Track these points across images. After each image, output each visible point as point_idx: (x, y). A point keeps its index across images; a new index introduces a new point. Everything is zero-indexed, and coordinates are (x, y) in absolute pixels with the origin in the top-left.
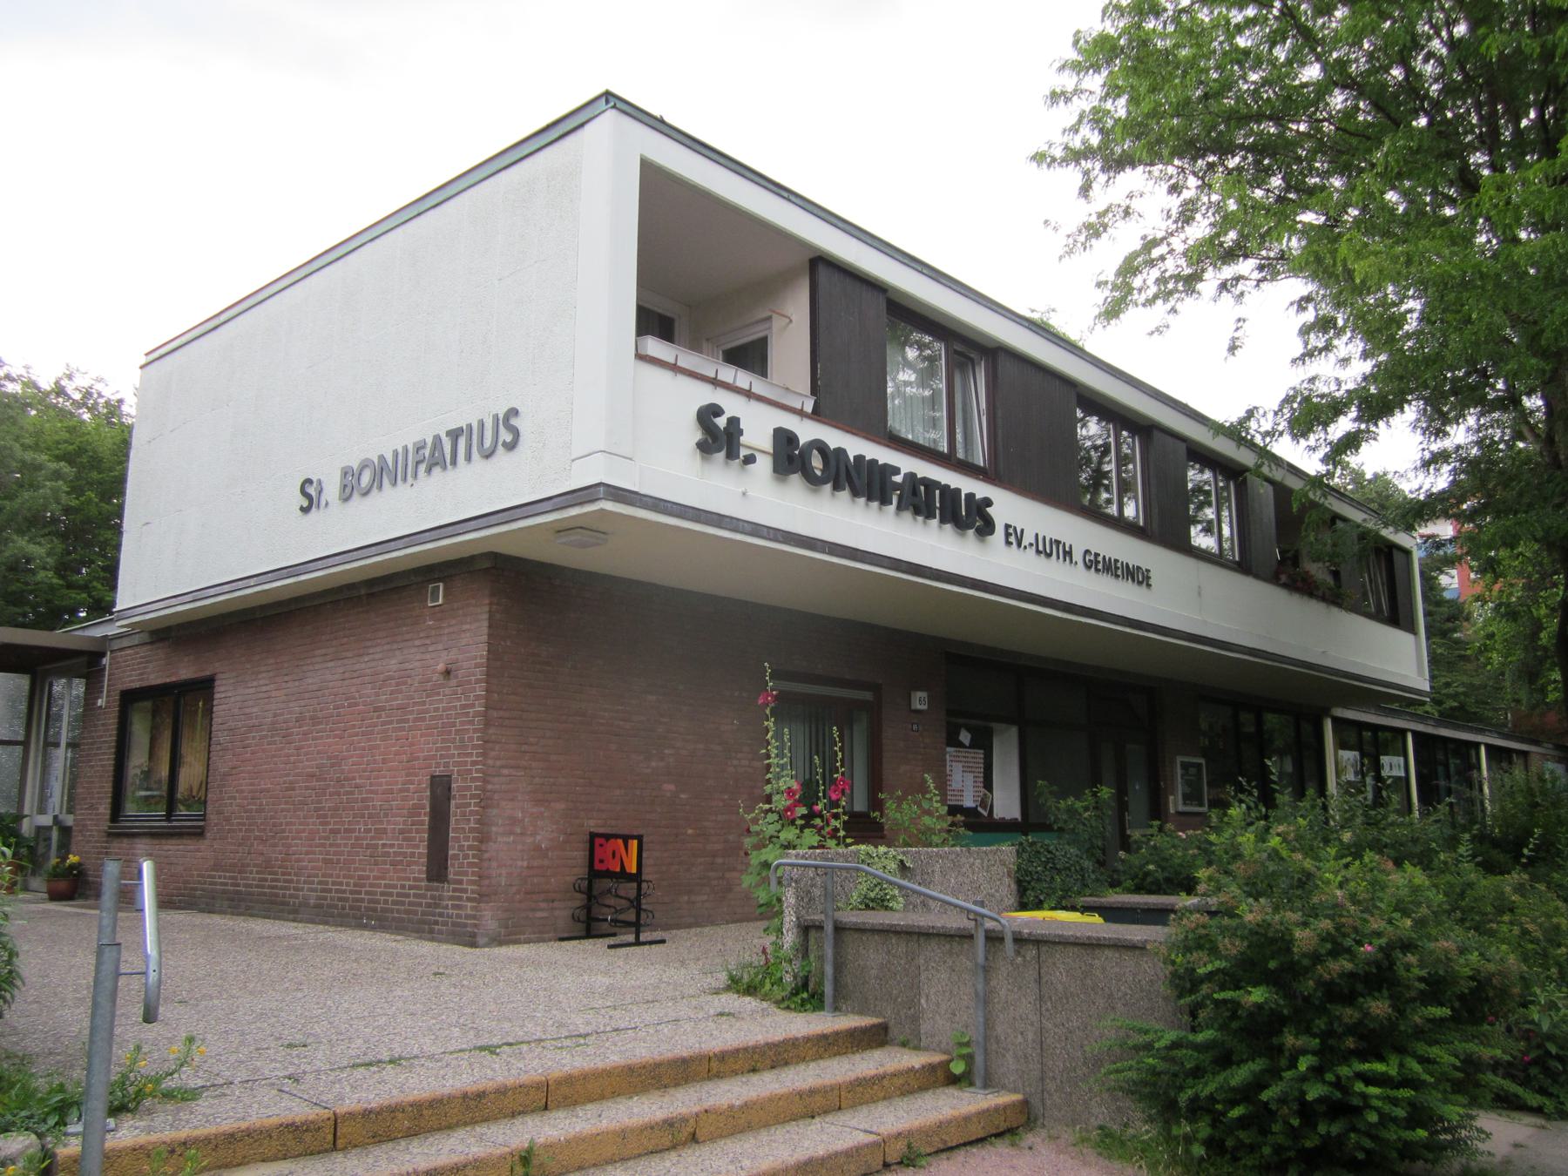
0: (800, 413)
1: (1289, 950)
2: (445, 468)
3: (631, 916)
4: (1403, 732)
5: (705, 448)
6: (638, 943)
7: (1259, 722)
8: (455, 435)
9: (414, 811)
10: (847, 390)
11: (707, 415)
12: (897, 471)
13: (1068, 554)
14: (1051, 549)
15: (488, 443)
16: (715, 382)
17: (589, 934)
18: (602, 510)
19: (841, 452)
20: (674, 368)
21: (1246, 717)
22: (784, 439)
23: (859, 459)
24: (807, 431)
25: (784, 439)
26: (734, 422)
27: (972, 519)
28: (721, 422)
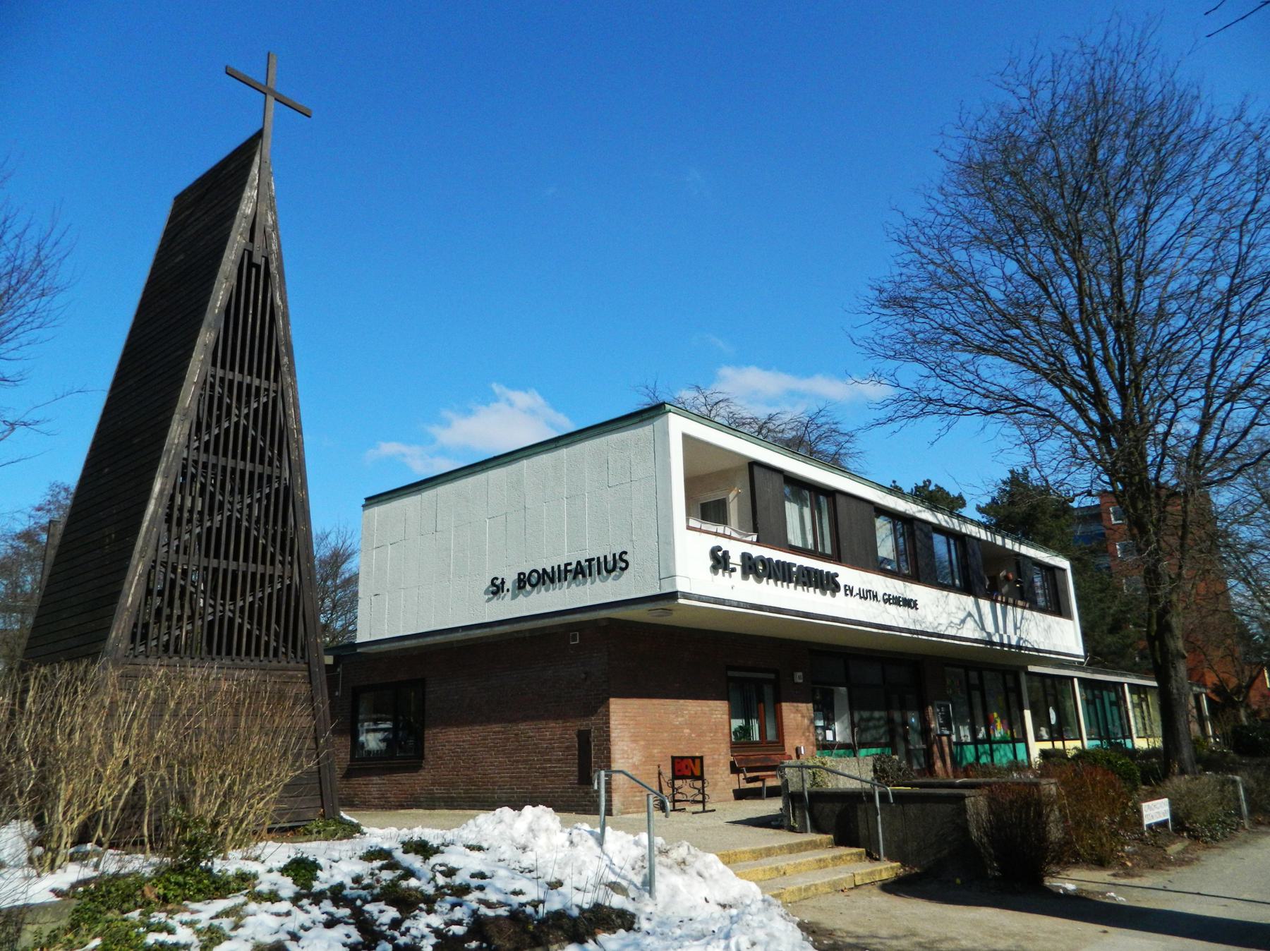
0: (751, 543)
3: (700, 798)
5: (714, 569)
6: (704, 811)
7: (981, 678)
8: (590, 561)
11: (714, 552)
13: (875, 596)
14: (868, 595)
16: (716, 534)
19: (770, 560)
20: (700, 530)
21: (973, 675)
22: (746, 557)
23: (778, 562)
24: (757, 551)
25: (746, 557)
26: (726, 553)
27: (827, 584)
28: (720, 553)
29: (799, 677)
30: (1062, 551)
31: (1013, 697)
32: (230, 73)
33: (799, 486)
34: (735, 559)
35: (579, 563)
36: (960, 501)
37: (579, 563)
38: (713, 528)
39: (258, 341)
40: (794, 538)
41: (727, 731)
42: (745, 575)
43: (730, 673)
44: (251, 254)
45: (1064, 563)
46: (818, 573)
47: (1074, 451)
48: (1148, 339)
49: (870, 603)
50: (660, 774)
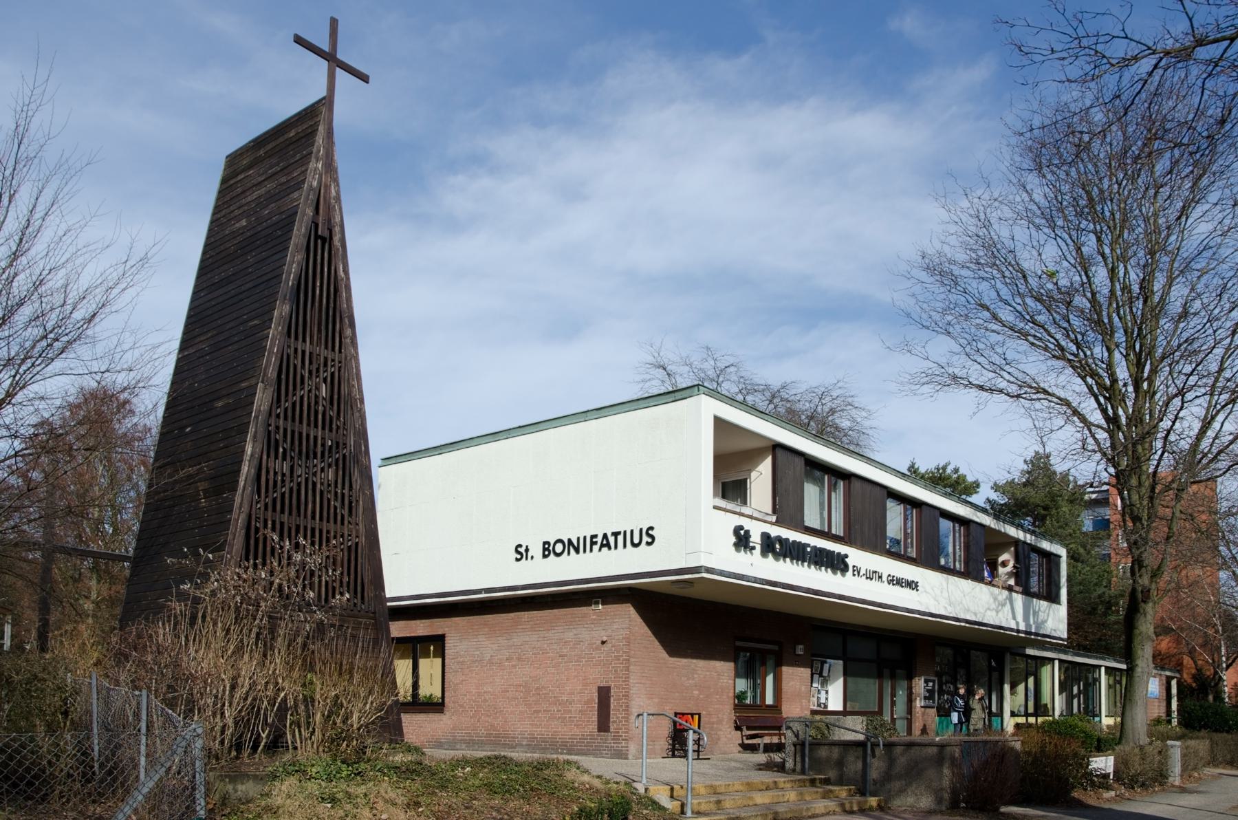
0: (770, 523)
1: (1145, 602)
2: (610, 548)
4: (1053, 659)
8: (616, 534)
9: (588, 702)
10: (786, 508)
11: (737, 530)
12: (808, 545)
13: (880, 577)
14: (873, 575)
15: (636, 541)
17: (674, 756)
18: (703, 578)
19: (787, 540)
22: (766, 537)
23: (794, 542)
24: (775, 531)
25: (766, 537)
26: (747, 532)
27: (837, 564)
29: (800, 650)
30: (1062, 541)
31: (995, 675)
32: (299, 40)
33: (815, 466)
34: (755, 538)
35: (605, 536)
36: (973, 488)
37: (605, 536)
38: (730, 506)
39: (326, 312)
40: (812, 518)
41: (731, 695)
42: (764, 553)
43: (738, 644)
44: (317, 226)
45: (1062, 552)
46: (829, 554)
47: (1084, 441)
48: (1164, 334)
49: (874, 584)
50: (981, 388)
